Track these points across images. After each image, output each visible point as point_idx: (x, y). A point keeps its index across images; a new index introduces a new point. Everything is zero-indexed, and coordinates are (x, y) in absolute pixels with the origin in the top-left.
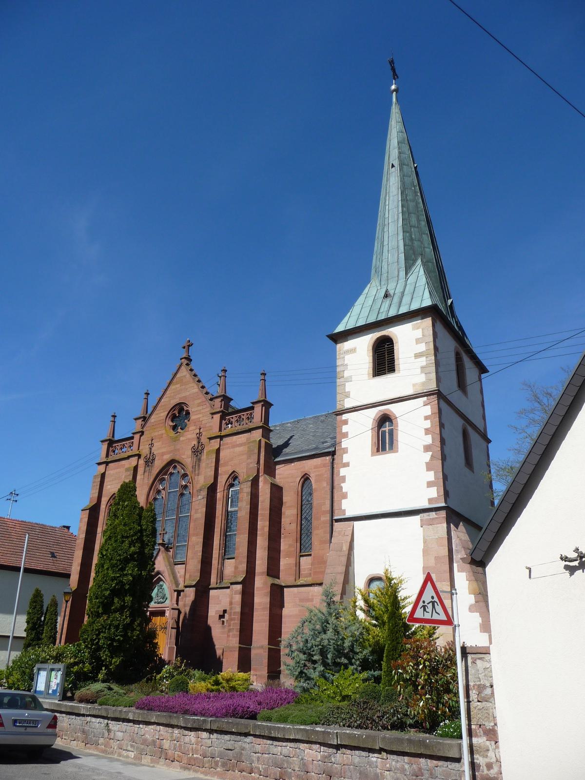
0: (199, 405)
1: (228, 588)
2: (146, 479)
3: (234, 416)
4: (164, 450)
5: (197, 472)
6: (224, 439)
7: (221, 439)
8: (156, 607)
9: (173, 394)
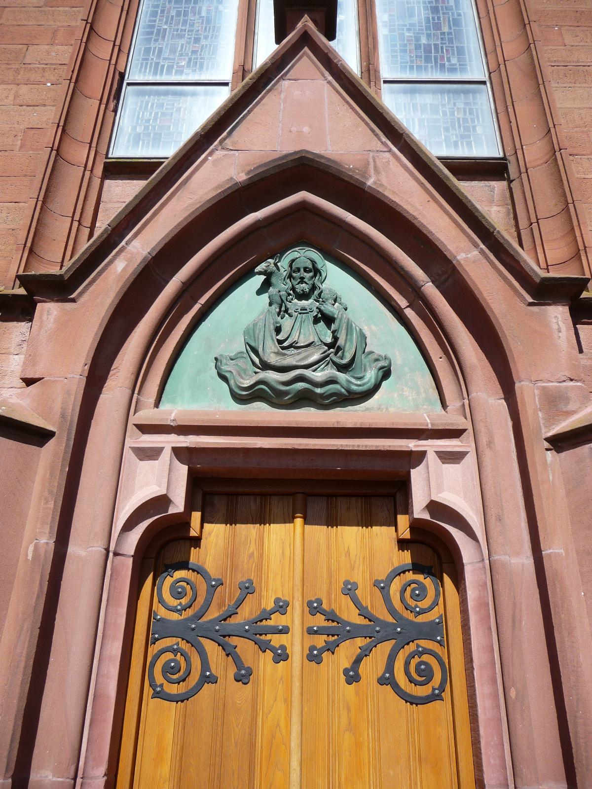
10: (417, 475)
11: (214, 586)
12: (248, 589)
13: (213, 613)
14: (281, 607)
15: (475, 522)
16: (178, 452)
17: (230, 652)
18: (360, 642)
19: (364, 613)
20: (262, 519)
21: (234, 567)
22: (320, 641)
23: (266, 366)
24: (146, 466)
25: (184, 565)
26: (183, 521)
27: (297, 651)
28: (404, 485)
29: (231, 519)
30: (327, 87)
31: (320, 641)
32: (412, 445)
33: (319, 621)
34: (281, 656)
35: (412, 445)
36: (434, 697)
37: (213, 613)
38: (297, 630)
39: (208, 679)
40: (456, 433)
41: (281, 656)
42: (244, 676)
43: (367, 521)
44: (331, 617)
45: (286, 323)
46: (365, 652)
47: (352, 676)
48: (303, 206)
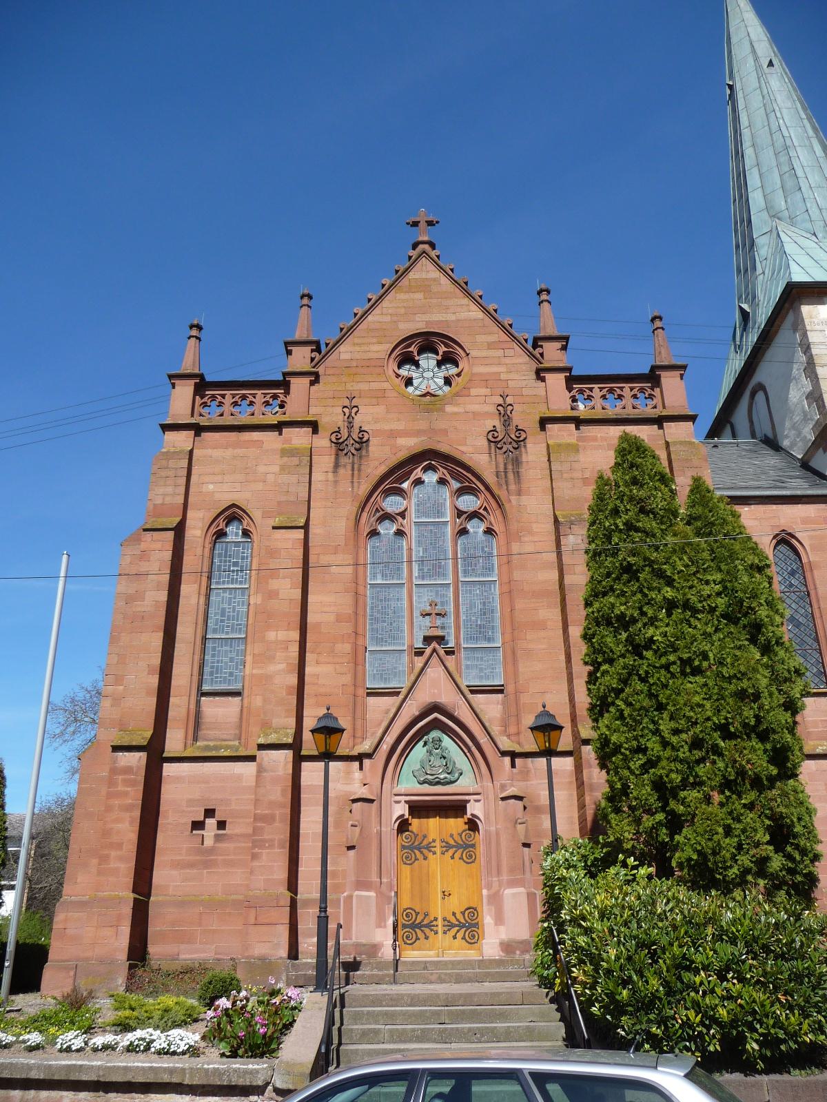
0: (490, 346)
1: (252, 758)
2: (345, 486)
3: (596, 386)
4: (399, 426)
5: (513, 487)
6: (203, 434)
7: (197, 434)
8: (415, 792)
9: (403, 311)
10: (468, 805)
11: (416, 836)
12: (425, 837)
13: (416, 843)
14: (434, 841)
15: (482, 818)
16: (406, 802)
17: (421, 852)
18: (454, 849)
19: (455, 842)
20: (428, 817)
21: (421, 831)
22: (444, 849)
23: (427, 774)
24: (397, 806)
25: (408, 831)
26: (407, 819)
27: (438, 853)
28: (465, 807)
29: (419, 818)
30: (442, 672)
31: (444, 849)
32: (467, 798)
33: (444, 844)
34: (434, 853)
35: (467, 798)
36: (473, 862)
37: (416, 843)
38: (438, 847)
39: (416, 859)
40: (479, 794)
41: (434, 853)
42: (425, 858)
43: (456, 817)
44: (447, 843)
45: (432, 758)
46: (456, 851)
47: (452, 858)
48: (436, 719)
